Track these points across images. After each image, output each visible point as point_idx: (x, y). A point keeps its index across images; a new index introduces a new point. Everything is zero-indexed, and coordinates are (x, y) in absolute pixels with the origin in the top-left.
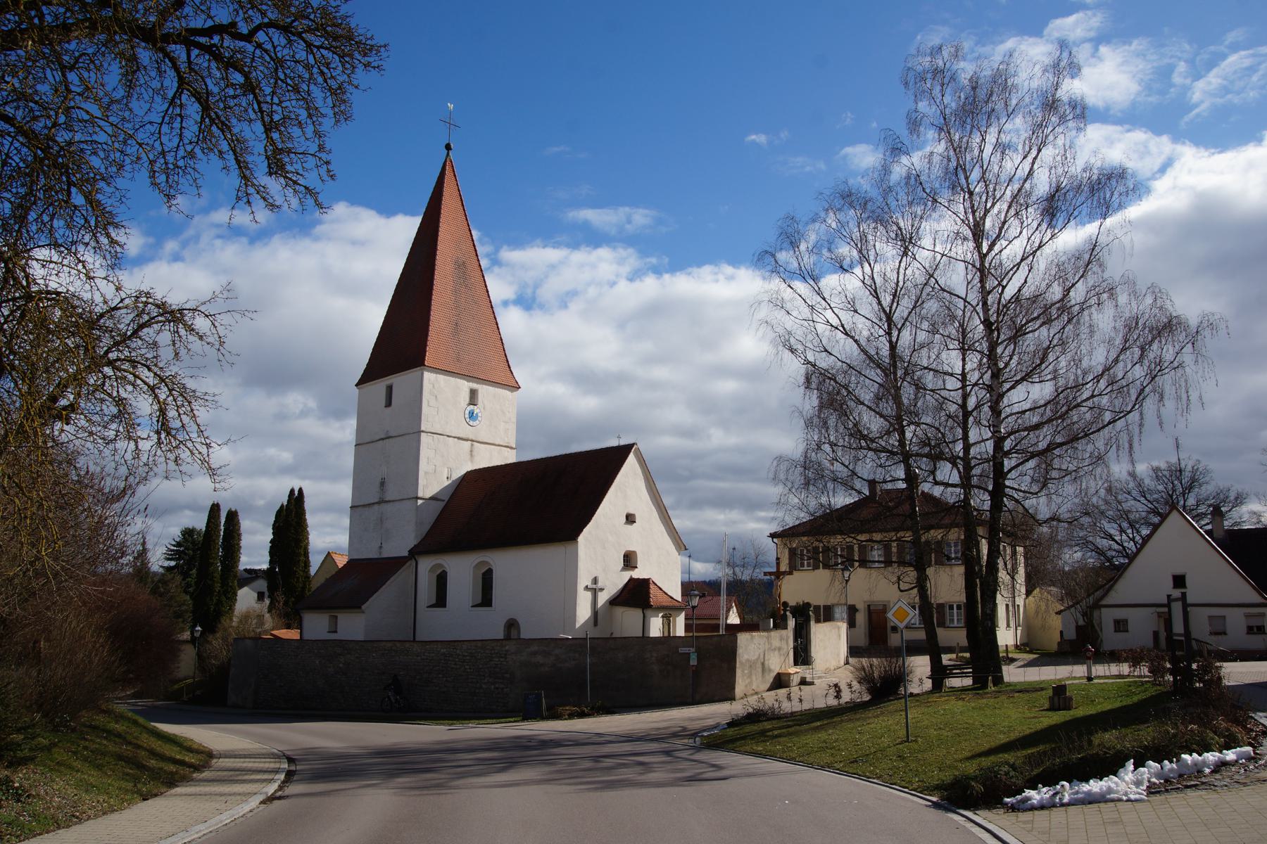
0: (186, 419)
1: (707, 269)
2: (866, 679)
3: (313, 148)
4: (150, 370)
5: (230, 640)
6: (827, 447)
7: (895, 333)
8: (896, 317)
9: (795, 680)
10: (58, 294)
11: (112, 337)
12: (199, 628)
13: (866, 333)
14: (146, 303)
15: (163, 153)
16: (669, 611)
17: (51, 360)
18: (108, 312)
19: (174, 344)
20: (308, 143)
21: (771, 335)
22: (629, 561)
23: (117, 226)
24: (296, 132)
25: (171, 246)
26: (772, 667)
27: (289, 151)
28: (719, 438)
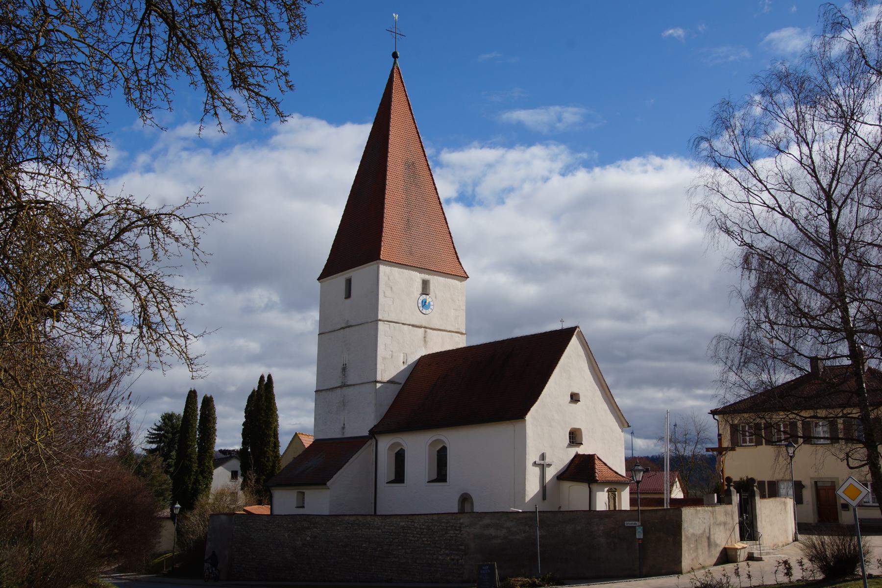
0: (165, 314)
1: (636, 162)
2: (817, 556)
3: (273, 61)
4: (131, 270)
5: (207, 516)
6: (767, 326)
7: (835, 211)
8: (836, 195)
9: (743, 555)
10: (46, 203)
11: (97, 241)
12: (178, 506)
13: (804, 213)
14: (126, 210)
15: (136, 72)
16: (614, 485)
17: (42, 263)
18: (92, 218)
19: (153, 246)
20: (268, 57)
21: (709, 218)
22: (575, 438)
23: (97, 139)
24: (256, 47)
25: (143, 158)
26: (718, 542)
27: (251, 65)
28: (653, 320)
